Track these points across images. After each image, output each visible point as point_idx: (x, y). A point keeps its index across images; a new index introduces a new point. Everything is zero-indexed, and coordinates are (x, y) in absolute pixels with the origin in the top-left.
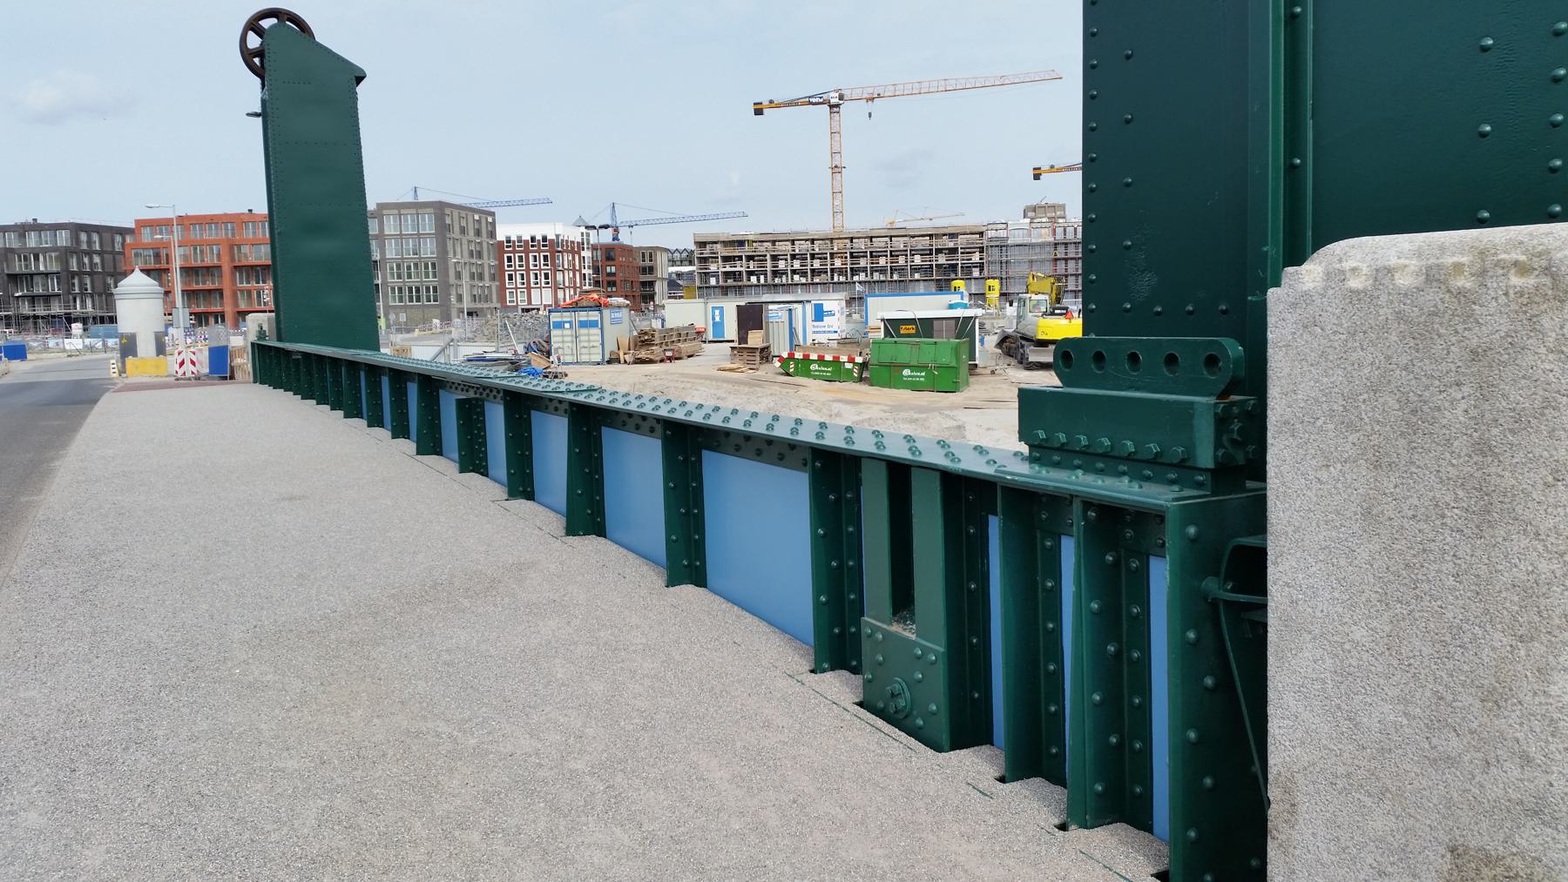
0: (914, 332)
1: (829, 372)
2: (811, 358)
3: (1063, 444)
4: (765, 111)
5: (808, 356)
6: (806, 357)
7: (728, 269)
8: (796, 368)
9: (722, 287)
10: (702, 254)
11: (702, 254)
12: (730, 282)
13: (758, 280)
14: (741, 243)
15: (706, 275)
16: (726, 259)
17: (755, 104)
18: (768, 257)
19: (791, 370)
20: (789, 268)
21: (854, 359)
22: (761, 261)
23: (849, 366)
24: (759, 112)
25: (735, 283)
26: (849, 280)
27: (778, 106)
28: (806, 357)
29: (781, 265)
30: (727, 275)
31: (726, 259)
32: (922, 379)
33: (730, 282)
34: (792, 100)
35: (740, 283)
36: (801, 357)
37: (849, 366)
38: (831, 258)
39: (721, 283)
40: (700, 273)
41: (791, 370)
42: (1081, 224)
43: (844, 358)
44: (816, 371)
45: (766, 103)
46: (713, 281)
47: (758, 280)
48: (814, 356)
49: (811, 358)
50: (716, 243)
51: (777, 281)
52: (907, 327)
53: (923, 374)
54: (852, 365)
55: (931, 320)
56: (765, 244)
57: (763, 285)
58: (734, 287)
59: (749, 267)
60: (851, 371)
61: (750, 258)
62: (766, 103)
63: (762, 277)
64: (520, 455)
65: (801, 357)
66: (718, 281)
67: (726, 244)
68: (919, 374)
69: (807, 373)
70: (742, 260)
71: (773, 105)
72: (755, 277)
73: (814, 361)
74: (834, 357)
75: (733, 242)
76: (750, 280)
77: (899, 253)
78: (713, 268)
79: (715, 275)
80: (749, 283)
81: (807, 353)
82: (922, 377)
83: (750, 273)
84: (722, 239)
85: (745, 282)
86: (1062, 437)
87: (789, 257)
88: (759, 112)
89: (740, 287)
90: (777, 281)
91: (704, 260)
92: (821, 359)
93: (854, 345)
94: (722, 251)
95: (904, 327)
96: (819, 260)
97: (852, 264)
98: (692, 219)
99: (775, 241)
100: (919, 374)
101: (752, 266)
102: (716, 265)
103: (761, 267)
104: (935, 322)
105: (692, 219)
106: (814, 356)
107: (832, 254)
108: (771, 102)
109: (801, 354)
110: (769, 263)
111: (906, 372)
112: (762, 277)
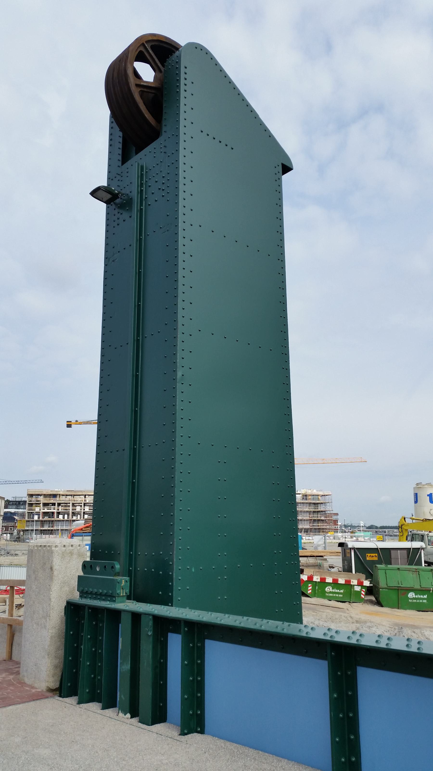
0: (376, 559)
1: (341, 593)
2: (327, 581)
3: (96, 592)
4: (73, 426)
5: (325, 579)
6: (323, 580)
7: (46, 510)
8: (314, 590)
9: (42, 521)
10: (31, 501)
11: (31, 501)
12: (46, 518)
13: (64, 517)
14: (55, 496)
15: (31, 514)
16: (45, 505)
17: (67, 422)
18: (71, 505)
19: (309, 592)
20: (82, 511)
21: (363, 582)
22: (65, 506)
23: (357, 588)
24: (69, 426)
25: (50, 519)
26: (41, 519)
27: (80, 424)
28: (323, 580)
29: (78, 509)
30: (45, 514)
31: (45, 505)
32: (425, 601)
33: (46, 518)
34: (88, 421)
35: (53, 519)
36: (319, 580)
37: (357, 588)
38: (84, 506)
39: (41, 519)
40: (29, 512)
41: (309, 592)
42: (90, 499)
43: (354, 582)
44: (330, 592)
45: (73, 421)
46: (36, 517)
47: (64, 517)
48: (329, 580)
49: (327, 581)
50: (41, 495)
51: (74, 518)
52: (372, 555)
53: (425, 597)
54: (360, 587)
55: (389, 550)
56: (68, 497)
57: (66, 521)
58: (49, 521)
59: (58, 510)
60: (359, 593)
61: (59, 504)
62: (73, 421)
63: (66, 516)
64: (191, 715)
65: (319, 580)
66: (39, 518)
67: (45, 496)
68: (422, 596)
69: (323, 595)
70: (55, 505)
71: (77, 423)
72: (62, 516)
73: (329, 584)
74: (346, 581)
75: (51, 495)
76: (58, 517)
77: (77, 504)
78: (37, 509)
79: (38, 513)
80: (58, 519)
81: (323, 577)
82: (424, 599)
83: (59, 513)
84: (45, 493)
85: (55, 518)
86: (101, 591)
87: (83, 505)
88: (69, 426)
89: (53, 521)
90: (74, 518)
91: (31, 505)
92: (335, 582)
93: (317, 567)
94: (42, 500)
95: (369, 555)
96: (88, 507)
97: (73, 510)
98: (25, 482)
99: (74, 495)
100: (422, 596)
101: (61, 509)
102: (39, 508)
103: (65, 510)
104: (392, 552)
105: (25, 482)
106: (329, 580)
107: (85, 504)
108: (77, 421)
109: (319, 577)
110: (71, 508)
111: (411, 595)
112: (66, 516)
